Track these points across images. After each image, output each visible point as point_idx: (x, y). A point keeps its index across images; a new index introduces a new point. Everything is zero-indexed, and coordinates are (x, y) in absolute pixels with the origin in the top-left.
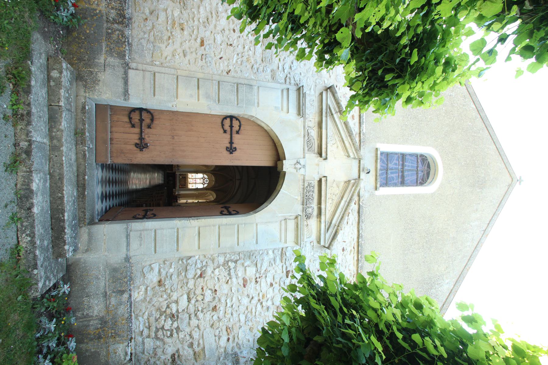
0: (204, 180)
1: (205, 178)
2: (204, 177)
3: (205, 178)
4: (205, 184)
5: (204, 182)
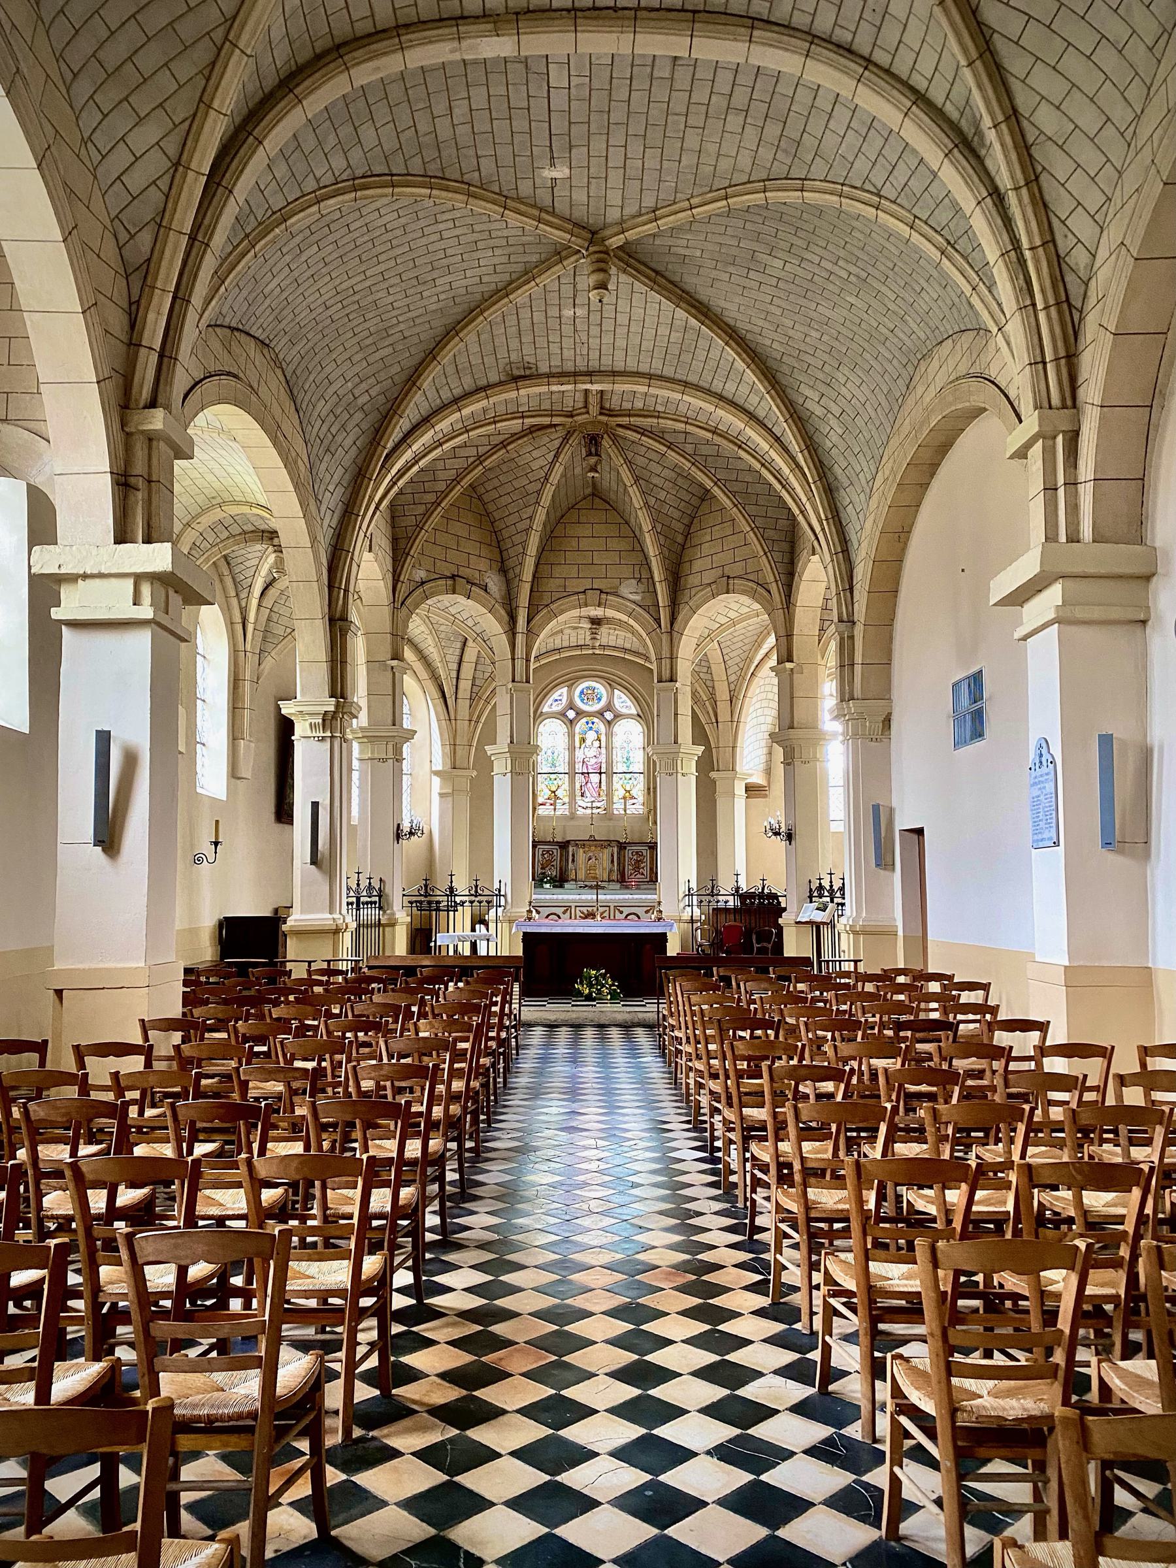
0: (580, 713)
1: (571, 706)
2: (562, 715)
3: (571, 706)
4: (609, 707)
5: (600, 714)
